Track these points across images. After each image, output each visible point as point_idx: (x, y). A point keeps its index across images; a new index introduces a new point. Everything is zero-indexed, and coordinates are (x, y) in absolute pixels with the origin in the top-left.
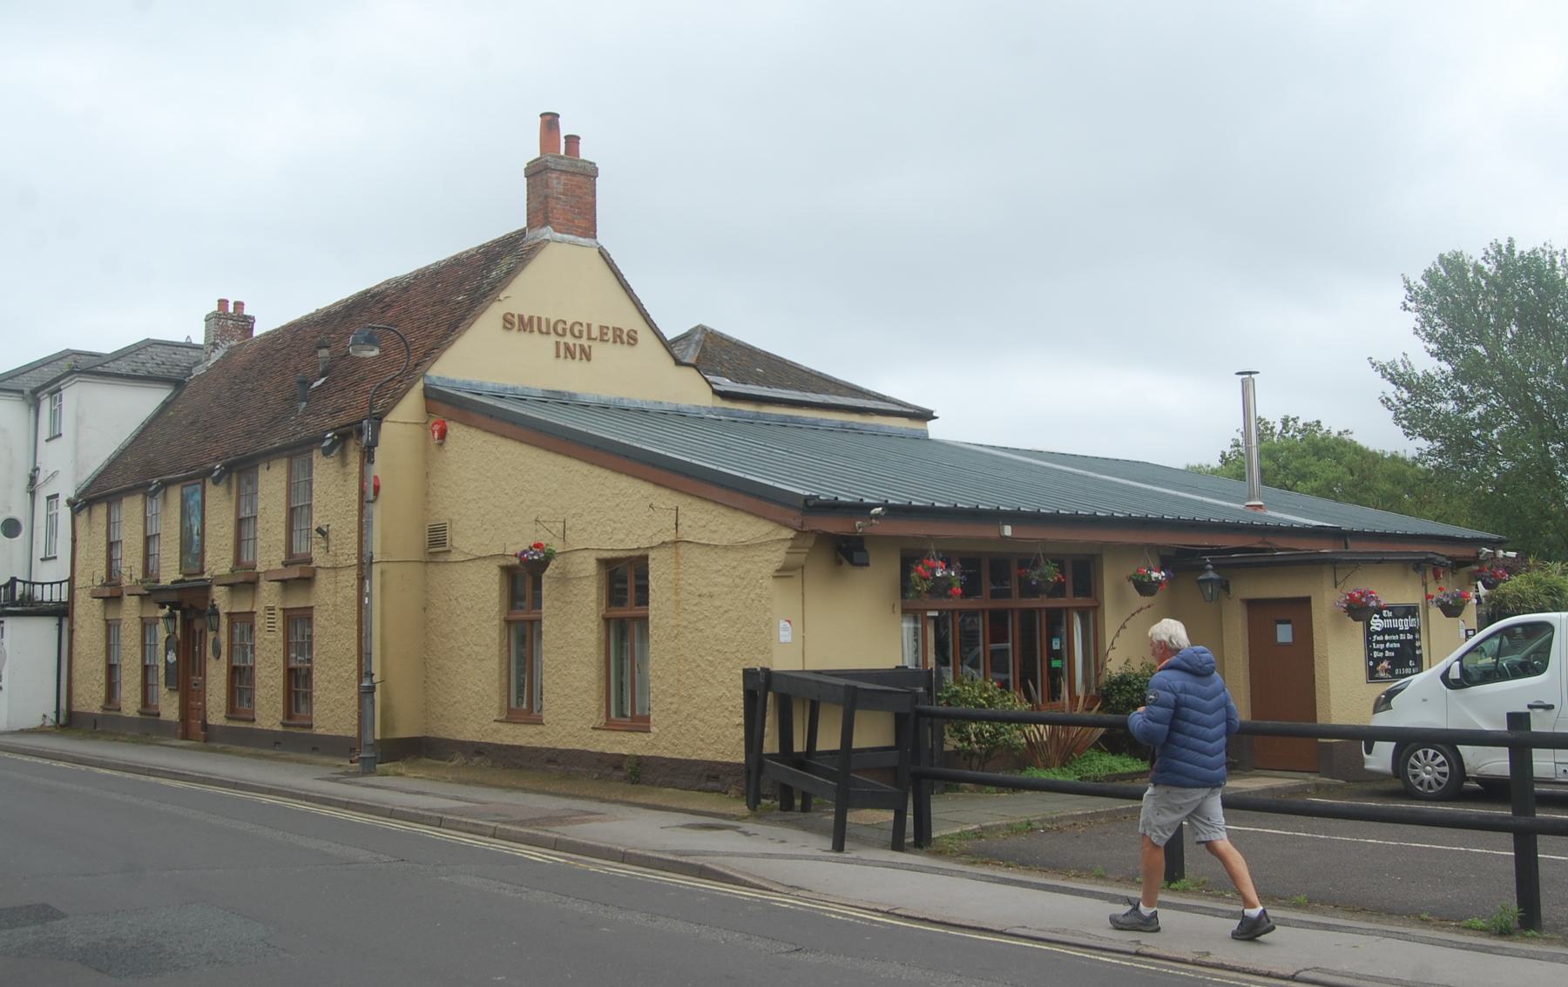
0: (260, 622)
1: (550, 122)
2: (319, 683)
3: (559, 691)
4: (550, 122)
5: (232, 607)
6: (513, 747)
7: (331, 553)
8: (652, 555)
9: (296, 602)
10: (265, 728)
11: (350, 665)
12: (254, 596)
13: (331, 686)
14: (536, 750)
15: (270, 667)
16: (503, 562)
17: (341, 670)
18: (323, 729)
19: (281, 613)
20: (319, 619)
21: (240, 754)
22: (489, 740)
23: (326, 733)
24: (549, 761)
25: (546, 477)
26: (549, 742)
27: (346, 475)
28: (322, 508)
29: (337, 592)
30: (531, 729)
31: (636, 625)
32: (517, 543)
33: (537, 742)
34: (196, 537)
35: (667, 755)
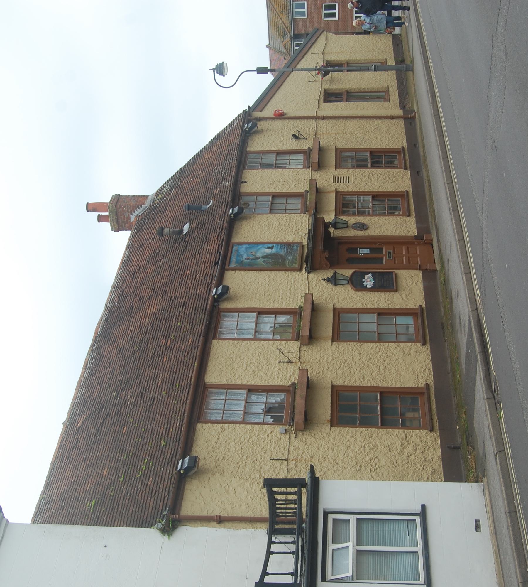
0: (342, 187)
1: (91, 207)
2: (378, 144)
3: (374, 82)
4: (91, 207)
5: (331, 211)
6: (399, 96)
7: (307, 138)
8: (326, 58)
9: (332, 158)
10: (411, 184)
11: (367, 126)
12: (326, 193)
13: (379, 137)
14: (399, 88)
15: (371, 180)
16: (322, 100)
17: (370, 131)
18: (404, 141)
19: (338, 170)
20: (343, 144)
21: (431, 200)
22: (398, 104)
23: (405, 139)
24: (402, 84)
25: (290, 88)
26: (395, 84)
27: (268, 130)
28: (282, 143)
29: (329, 133)
30: (391, 90)
31: (340, 217)
32: (315, 96)
33: (395, 87)
34: (274, 251)
35: (393, 54)
